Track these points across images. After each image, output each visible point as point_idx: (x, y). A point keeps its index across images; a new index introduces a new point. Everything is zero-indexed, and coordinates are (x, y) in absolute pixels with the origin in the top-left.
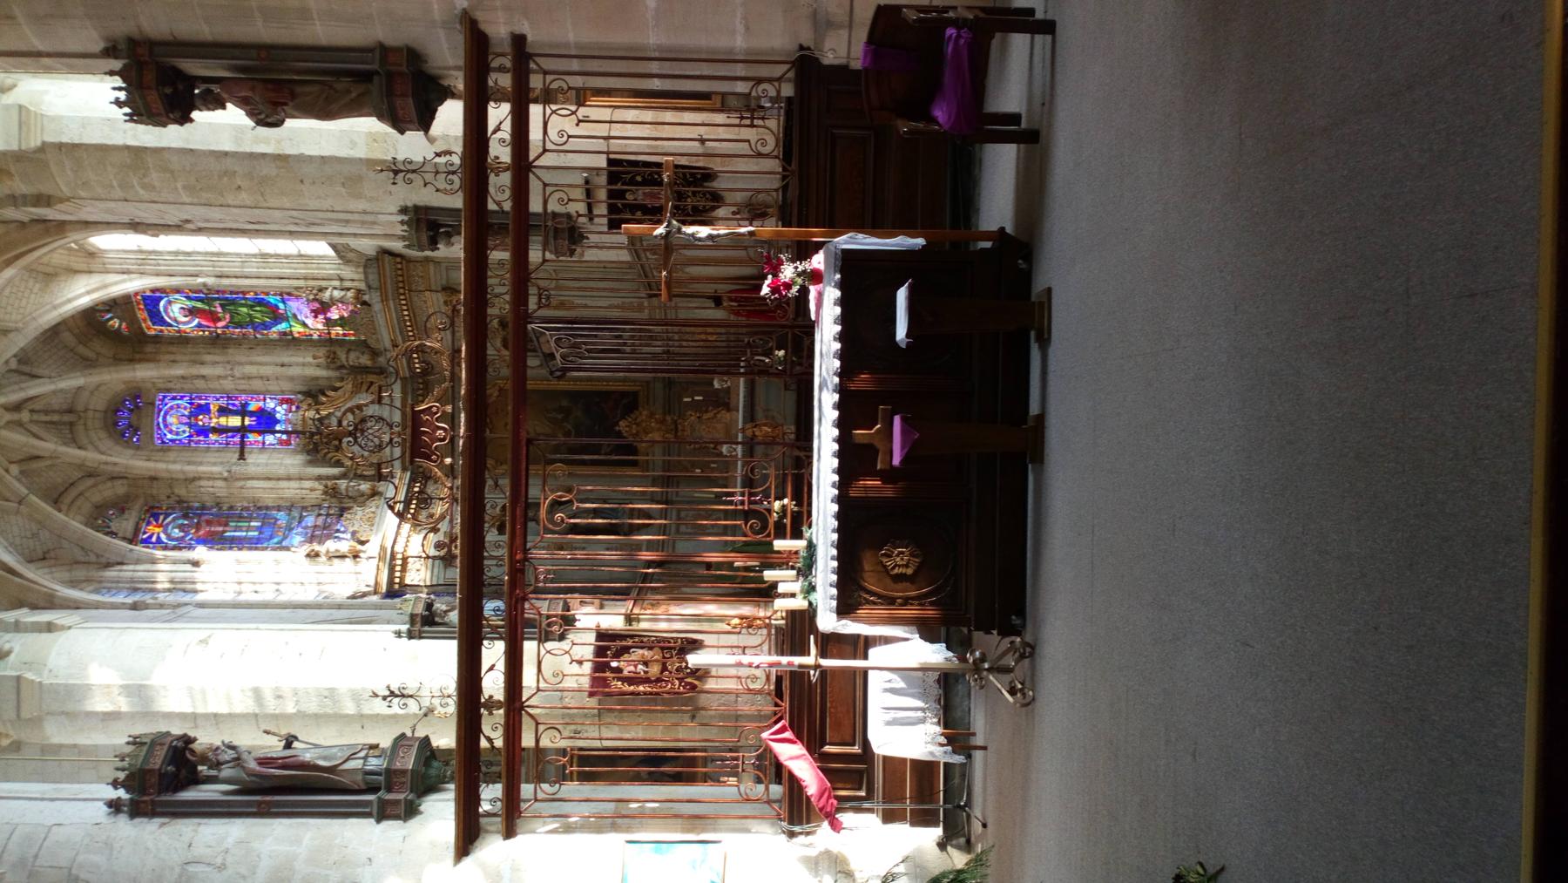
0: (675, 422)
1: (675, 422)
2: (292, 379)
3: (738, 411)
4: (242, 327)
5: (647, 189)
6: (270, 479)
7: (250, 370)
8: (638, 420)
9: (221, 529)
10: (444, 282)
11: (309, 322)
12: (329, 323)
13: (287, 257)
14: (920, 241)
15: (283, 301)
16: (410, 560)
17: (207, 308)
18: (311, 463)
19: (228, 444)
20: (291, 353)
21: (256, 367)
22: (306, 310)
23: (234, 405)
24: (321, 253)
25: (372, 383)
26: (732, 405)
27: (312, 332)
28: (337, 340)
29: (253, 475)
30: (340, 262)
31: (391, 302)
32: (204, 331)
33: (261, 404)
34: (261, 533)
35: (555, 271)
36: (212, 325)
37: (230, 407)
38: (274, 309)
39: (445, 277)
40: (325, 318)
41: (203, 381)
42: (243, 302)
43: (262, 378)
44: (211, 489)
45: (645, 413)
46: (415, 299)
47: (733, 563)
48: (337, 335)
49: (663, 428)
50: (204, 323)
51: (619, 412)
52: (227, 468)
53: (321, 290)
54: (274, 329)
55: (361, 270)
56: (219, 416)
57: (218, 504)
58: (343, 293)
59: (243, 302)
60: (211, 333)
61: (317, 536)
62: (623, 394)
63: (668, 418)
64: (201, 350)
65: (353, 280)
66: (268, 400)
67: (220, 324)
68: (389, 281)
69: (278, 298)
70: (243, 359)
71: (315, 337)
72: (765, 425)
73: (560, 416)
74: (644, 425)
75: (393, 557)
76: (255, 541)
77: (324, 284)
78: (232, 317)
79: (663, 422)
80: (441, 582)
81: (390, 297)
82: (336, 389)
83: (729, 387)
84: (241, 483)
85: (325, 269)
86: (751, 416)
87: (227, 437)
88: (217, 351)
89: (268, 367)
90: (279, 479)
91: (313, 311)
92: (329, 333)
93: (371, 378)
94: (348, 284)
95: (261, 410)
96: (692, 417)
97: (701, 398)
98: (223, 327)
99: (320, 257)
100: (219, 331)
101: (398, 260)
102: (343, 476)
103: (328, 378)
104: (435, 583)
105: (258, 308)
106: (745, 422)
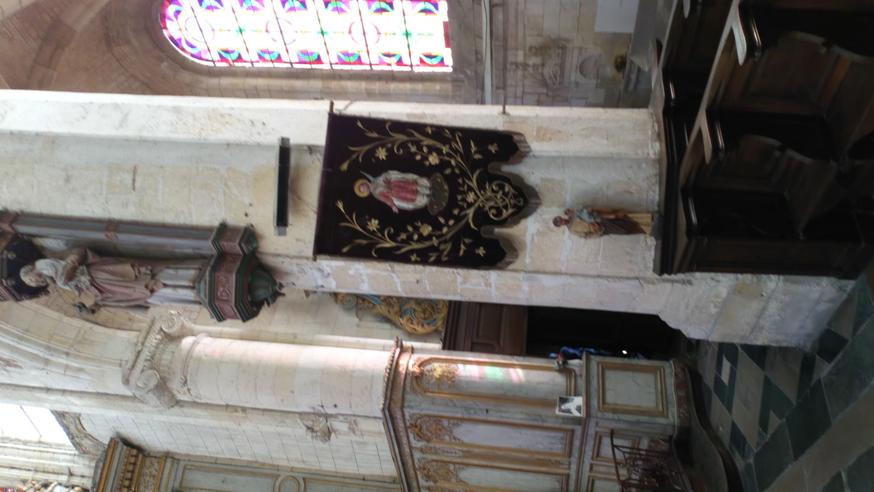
5: (394, 175)
13: (25, 443)
14: (472, 142)
24: (60, 442)
30: (77, 452)
35: (304, 479)
47: (249, 302)
55: (93, 464)
65: (83, 476)
68: (112, 474)
77: (51, 477)
85: (58, 460)
94: (76, 481)
99: (59, 446)
101: (134, 452)
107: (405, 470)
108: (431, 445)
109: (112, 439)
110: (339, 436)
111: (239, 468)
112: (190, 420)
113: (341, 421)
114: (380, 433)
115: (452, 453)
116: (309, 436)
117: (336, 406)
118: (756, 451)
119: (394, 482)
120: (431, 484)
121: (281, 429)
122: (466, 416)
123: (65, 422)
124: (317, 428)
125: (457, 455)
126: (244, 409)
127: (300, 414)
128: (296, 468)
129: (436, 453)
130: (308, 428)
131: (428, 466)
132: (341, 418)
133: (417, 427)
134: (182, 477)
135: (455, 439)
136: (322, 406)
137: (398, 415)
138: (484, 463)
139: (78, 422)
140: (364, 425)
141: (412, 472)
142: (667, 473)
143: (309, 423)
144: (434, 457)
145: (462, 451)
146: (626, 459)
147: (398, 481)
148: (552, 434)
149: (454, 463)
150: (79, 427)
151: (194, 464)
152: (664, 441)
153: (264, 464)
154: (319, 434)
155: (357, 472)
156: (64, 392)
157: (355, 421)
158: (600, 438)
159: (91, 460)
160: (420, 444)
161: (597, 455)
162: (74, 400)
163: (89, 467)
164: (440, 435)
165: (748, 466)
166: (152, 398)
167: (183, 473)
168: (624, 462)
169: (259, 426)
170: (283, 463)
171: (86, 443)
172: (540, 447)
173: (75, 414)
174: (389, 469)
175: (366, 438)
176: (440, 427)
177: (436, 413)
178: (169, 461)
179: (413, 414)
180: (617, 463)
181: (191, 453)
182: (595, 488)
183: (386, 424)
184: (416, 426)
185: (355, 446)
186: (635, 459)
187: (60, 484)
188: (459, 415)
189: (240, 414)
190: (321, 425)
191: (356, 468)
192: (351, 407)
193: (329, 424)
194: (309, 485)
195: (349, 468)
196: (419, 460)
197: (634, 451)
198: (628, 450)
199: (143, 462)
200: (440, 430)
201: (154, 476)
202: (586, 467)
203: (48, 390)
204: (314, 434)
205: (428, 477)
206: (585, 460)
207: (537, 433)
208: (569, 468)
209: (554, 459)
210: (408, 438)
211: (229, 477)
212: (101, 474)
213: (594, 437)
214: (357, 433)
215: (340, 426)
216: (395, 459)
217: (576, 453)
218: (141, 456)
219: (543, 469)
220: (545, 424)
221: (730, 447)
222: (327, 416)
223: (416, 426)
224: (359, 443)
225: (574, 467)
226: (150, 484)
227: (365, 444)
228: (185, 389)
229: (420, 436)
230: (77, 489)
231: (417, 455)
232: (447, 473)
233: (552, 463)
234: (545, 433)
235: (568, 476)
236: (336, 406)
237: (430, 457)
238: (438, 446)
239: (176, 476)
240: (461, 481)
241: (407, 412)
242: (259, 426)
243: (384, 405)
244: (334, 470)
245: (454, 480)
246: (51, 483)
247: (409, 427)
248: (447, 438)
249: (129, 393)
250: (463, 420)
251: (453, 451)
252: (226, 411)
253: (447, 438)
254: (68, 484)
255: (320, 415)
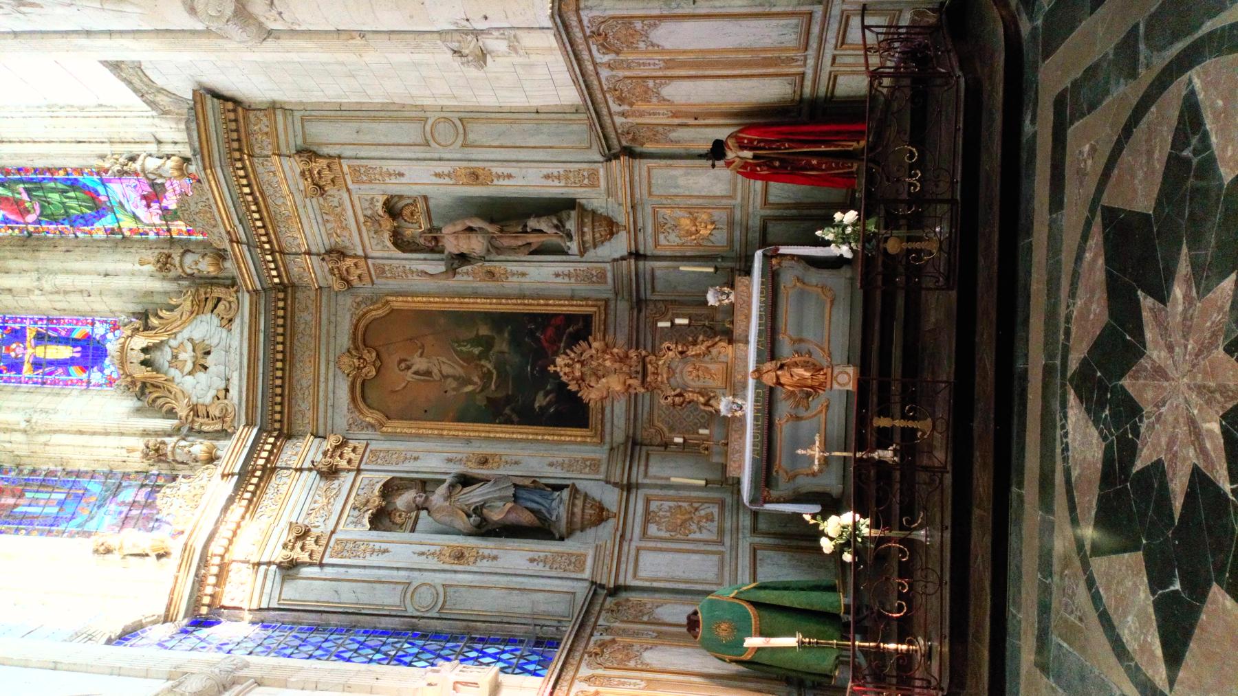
0: (643, 361)
1: (643, 361)
2: (119, 294)
3: (747, 342)
4: (57, 223)
6: (81, 432)
7: (63, 281)
8: (586, 356)
9: (11, 501)
10: (300, 141)
11: (141, 212)
12: (166, 213)
15: (103, 182)
16: (233, 567)
17: (10, 194)
18: (139, 411)
19: (44, 383)
20: (118, 257)
21: (71, 277)
22: (134, 196)
23: (55, 330)
25: (219, 300)
26: (738, 332)
27: (147, 228)
28: (180, 240)
29: (60, 427)
30: (154, 113)
31: (219, 170)
32: (12, 229)
33: (88, 329)
34: (61, 509)
35: (460, 119)
36: (20, 220)
37: (50, 333)
38: (93, 195)
39: (300, 133)
40: (160, 208)
41: (9, 297)
42: (52, 184)
43: (81, 292)
44: (8, 445)
45: (595, 345)
46: (260, 169)
48: (180, 232)
49: (625, 369)
50: (12, 217)
51: (562, 345)
52: (27, 417)
53: (133, 159)
54: (98, 225)
55: (183, 126)
56: (36, 345)
57: (18, 466)
58: (160, 162)
59: (52, 184)
60: (21, 231)
61: (132, 518)
62: (570, 318)
63: (633, 354)
64: (7, 254)
66: (97, 325)
67: (31, 218)
69: (96, 178)
70: (56, 265)
71: (152, 236)
72: (796, 365)
73: (476, 351)
74: (594, 363)
75: (204, 561)
76: (51, 521)
77: (135, 149)
78: (42, 207)
79: (624, 359)
80: (274, 605)
81: (217, 163)
82: (171, 308)
83: (732, 305)
84: (43, 438)
86: (770, 351)
87: (45, 374)
88: (25, 254)
89: (88, 277)
90: (94, 433)
91: (144, 197)
92: (169, 230)
93: (218, 292)
94: (168, 149)
95: (88, 337)
96: (670, 353)
97: (685, 321)
98: (34, 223)
100: (31, 228)
101: (230, 105)
102: (176, 431)
103: (166, 293)
104: (264, 605)
105: (72, 194)
106: (760, 360)
107: (590, 95)
108: (622, 57)
109: (194, 92)
110: (497, 59)
111: (373, 114)
112: (294, 56)
113: (497, 38)
114: (550, 49)
115: (649, 64)
116: (456, 62)
117: (486, 18)
118: (1047, 8)
119: (577, 112)
120: (626, 108)
121: (417, 57)
122: (665, 13)
123: (124, 75)
124: (466, 51)
125: (657, 67)
126: (362, 34)
127: (439, 33)
128: (447, 107)
129: (629, 67)
130: (455, 52)
131: (619, 85)
132: (496, 34)
133: (599, 35)
134: (304, 133)
135: (653, 45)
136: (468, 20)
137: (573, 22)
138: (692, 73)
139: (140, 73)
140: (528, 40)
141: (599, 96)
142: (931, 53)
143: (455, 45)
144: (627, 73)
145: (664, 61)
146: (879, 43)
147: (583, 109)
148: (783, 22)
149: (654, 78)
150: (145, 79)
151: (313, 113)
152: (933, 10)
153: (404, 106)
154: (470, 58)
155: (527, 104)
156: (110, 33)
157: (515, 36)
158: (848, 18)
159: (178, 121)
160: (606, 58)
161: (842, 41)
162: (127, 42)
163: (179, 130)
164: (632, 43)
165: (1035, 28)
166: (233, 30)
167: (303, 127)
168: (876, 47)
169: (387, 55)
170: (428, 102)
171: (161, 99)
172: (767, 42)
173: (133, 62)
174: (570, 95)
175: (534, 58)
176: (631, 31)
177: (625, 13)
178: (279, 112)
179: (594, 18)
180: (867, 49)
181: (304, 100)
182: (837, 85)
183: (558, 35)
184: (599, 35)
185: (519, 70)
186: (893, 40)
187: (150, 155)
188: (656, 12)
189: (358, 41)
190: (472, 46)
191: (525, 99)
192: (507, 17)
193: (480, 43)
194: (469, 126)
195: (516, 100)
196: (607, 79)
197: (892, 30)
198: (884, 30)
199: (245, 118)
200: (632, 35)
201: (267, 133)
202: (828, 60)
203: (88, 33)
204: (464, 59)
205: (621, 100)
206: (826, 51)
207: (762, 22)
208: (805, 65)
209: (784, 55)
210: (590, 51)
211: (364, 125)
212: (199, 137)
213: (839, 18)
214: (521, 52)
215: (496, 44)
216: (576, 81)
217: (814, 44)
218: (240, 110)
219: (771, 70)
220: (774, 10)
221: (1018, 9)
222: (477, 33)
223: (599, 35)
224: (523, 65)
225: (811, 62)
226: (265, 144)
227: (532, 65)
228: (274, 12)
229: (606, 48)
230: (173, 158)
231: (605, 73)
232: (646, 92)
233: (783, 61)
234: (775, 22)
235: (803, 75)
236: (486, 18)
237: (621, 74)
238: (630, 58)
239: (294, 131)
240: (664, 100)
241: (585, 16)
242: (387, 55)
243: (552, 8)
244: (497, 104)
245: (654, 100)
246: (139, 155)
247: (590, 37)
248: (642, 45)
249: (200, 26)
250: (662, 18)
251: (652, 62)
252: (338, 38)
253: (642, 45)
254: (160, 155)
255: (466, 32)
